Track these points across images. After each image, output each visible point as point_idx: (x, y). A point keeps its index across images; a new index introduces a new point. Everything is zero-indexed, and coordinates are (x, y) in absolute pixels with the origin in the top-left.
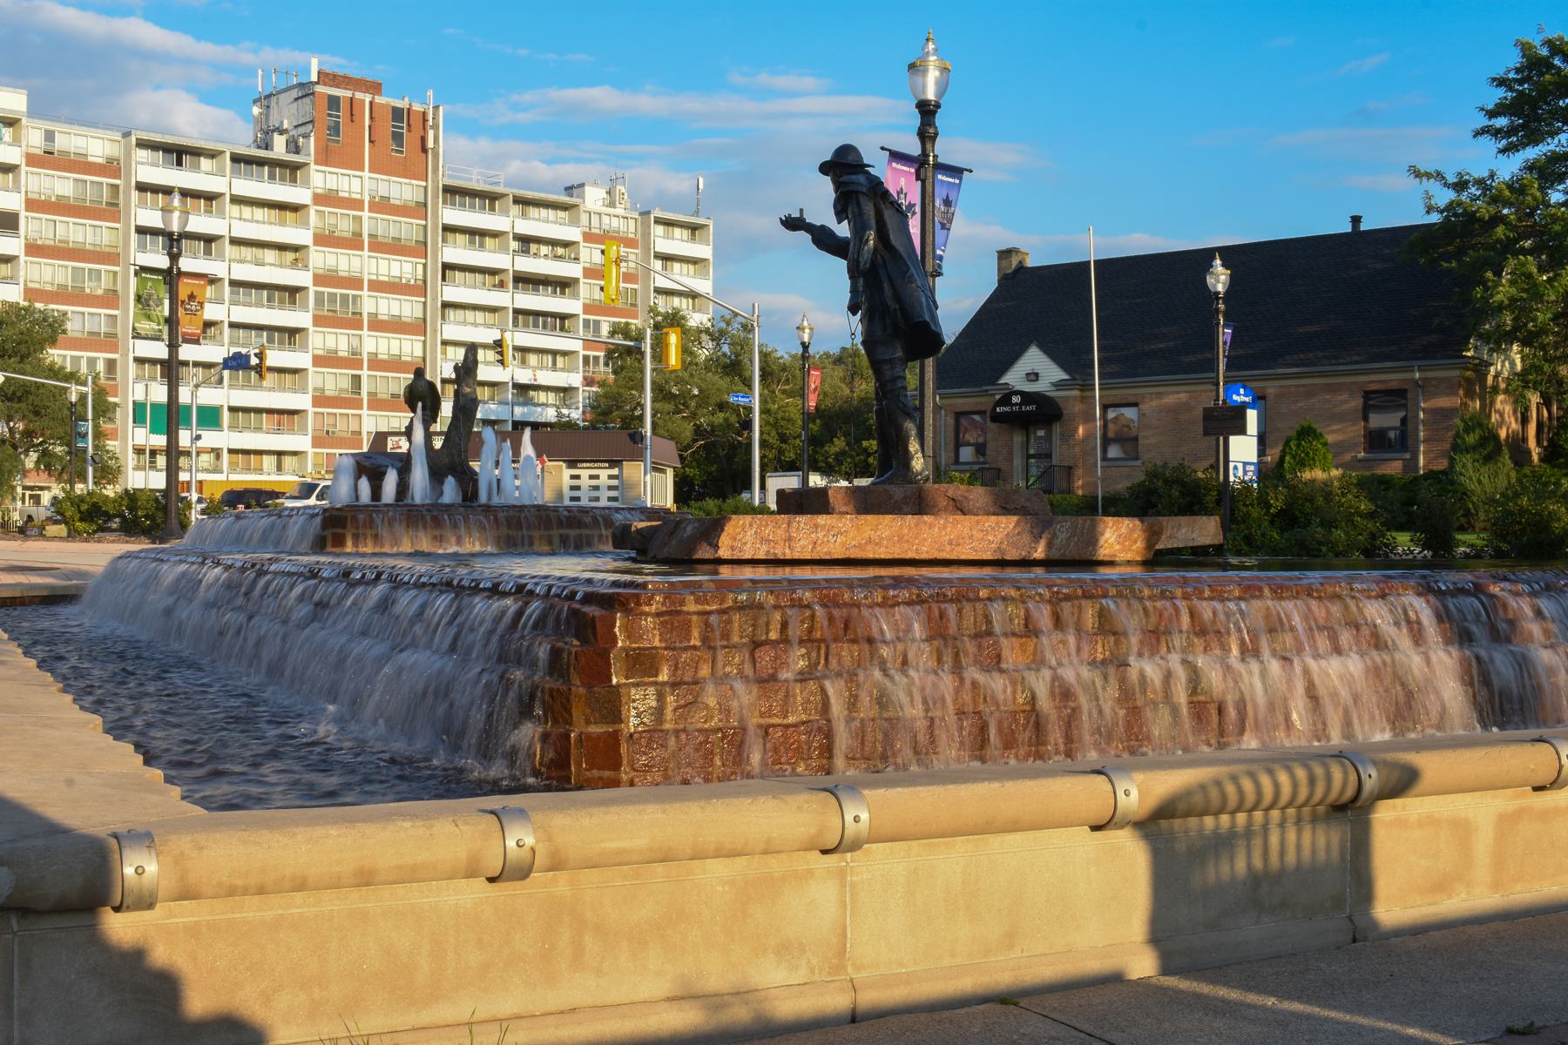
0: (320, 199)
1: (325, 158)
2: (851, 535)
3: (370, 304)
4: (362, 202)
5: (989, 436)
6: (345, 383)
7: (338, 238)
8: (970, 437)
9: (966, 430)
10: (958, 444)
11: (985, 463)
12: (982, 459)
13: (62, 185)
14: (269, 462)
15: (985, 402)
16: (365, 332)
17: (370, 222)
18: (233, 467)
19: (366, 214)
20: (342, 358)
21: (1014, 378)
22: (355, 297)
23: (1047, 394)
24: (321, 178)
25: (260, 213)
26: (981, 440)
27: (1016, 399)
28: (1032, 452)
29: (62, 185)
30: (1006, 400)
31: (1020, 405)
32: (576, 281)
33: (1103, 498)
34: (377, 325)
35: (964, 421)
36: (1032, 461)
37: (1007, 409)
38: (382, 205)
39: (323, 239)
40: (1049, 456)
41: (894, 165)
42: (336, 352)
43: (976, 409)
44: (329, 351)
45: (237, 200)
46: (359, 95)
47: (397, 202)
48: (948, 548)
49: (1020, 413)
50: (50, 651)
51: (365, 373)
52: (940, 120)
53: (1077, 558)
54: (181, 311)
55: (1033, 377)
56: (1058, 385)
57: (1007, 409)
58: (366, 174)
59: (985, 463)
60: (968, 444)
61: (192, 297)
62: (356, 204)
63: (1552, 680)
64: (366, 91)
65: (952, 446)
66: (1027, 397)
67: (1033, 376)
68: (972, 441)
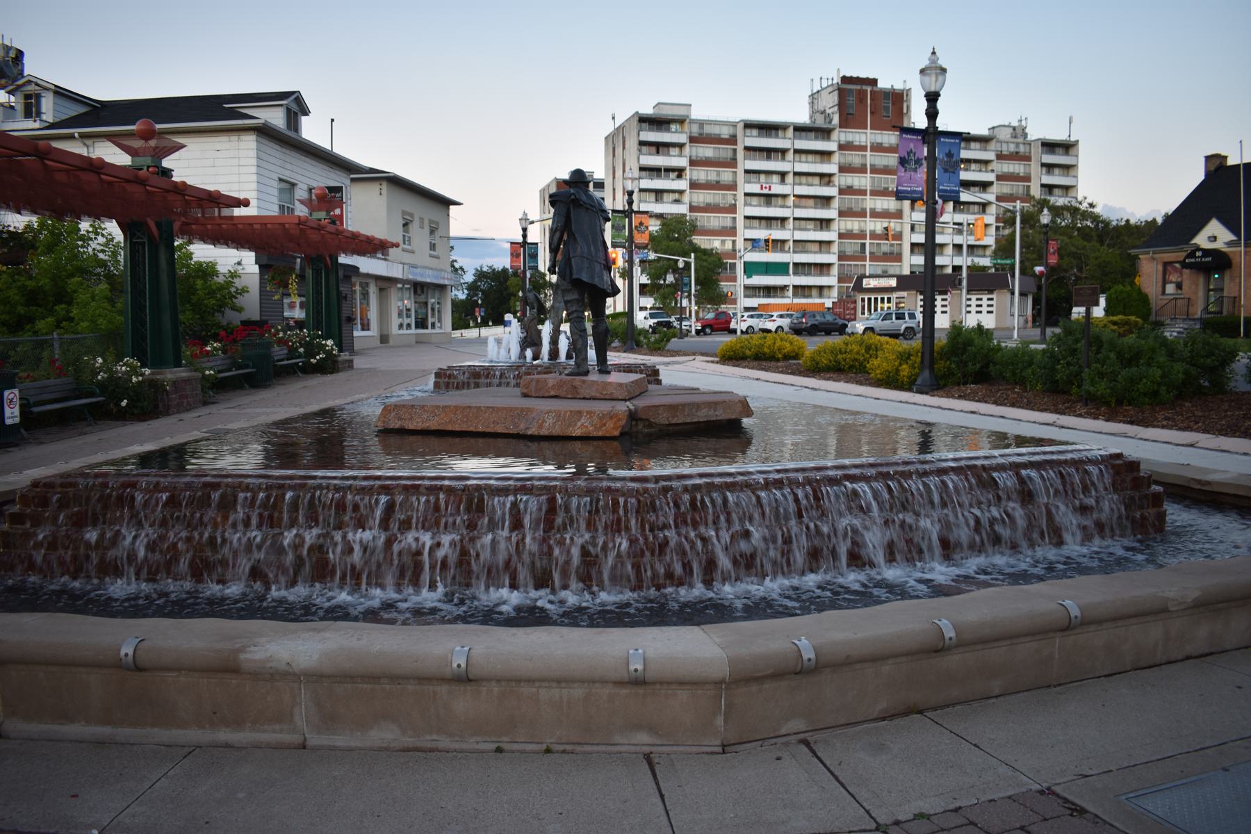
0: (842, 147)
1: (844, 124)
2: (442, 416)
3: (870, 203)
4: (866, 147)
5: (1185, 277)
6: (858, 248)
7: (853, 168)
8: (1173, 278)
9: (1170, 273)
10: (1165, 283)
11: (1181, 294)
12: (1180, 292)
13: (707, 151)
14: (814, 292)
15: (1181, 256)
16: (868, 219)
17: (871, 158)
18: (795, 295)
19: (868, 153)
20: (855, 234)
21: (1201, 240)
22: (862, 199)
23: (1223, 250)
24: (841, 136)
25: (810, 157)
26: (1179, 280)
27: (1198, 254)
28: (1211, 287)
29: (707, 151)
30: (1192, 255)
31: (1201, 257)
32: (991, 183)
33: (1245, 318)
34: (875, 214)
35: (1169, 268)
36: (1212, 293)
37: (1193, 260)
38: (877, 148)
39: (843, 169)
40: (1222, 290)
41: (904, 136)
42: (852, 231)
43: (1176, 260)
44: (848, 230)
45: (797, 151)
46: (864, 87)
47: (887, 145)
48: (492, 425)
49: (1201, 262)
50: (283, 435)
51: (868, 242)
52: (940, 104)
53: (561, 434)
54: (635, 232)
55: (1212, 239)
56: (1230, 244)
57: (1193, 260)
58: (869, 131)
59: (1181, 294)
60: (1171, 282)
61: (641, 224)
62: (863, 148)
63: (379, 581)
64: (867, 85)
65: (1160, 284)
66: (1206, 252)
67: (1214, 239)
68: (1174, 280)
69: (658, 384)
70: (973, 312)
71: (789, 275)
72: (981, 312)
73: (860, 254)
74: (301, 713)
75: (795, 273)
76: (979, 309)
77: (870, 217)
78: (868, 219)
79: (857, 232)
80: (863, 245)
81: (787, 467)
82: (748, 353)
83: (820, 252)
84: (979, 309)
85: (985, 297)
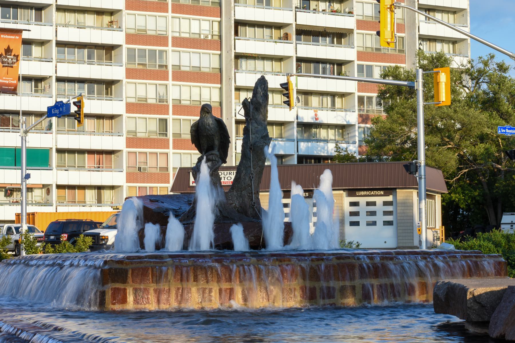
14: (90, 195)
22: (161, 52)
44: (140, 99)
51: (170, 117)
69: (135, 288)
70: (380, 223)
71: (22, 111)
72: (374, 223)
73: (158, 137)
74: (154, 262)
75: (61, 166)
76: (372, 219)
77: (174, 80)
78: (170, 82)
79: (153, 101)
80: (164, 123)
81: (100, 314)
82: (170, 299)
83: (99, 168)
84: (372, 219)
85: (379, 200)
